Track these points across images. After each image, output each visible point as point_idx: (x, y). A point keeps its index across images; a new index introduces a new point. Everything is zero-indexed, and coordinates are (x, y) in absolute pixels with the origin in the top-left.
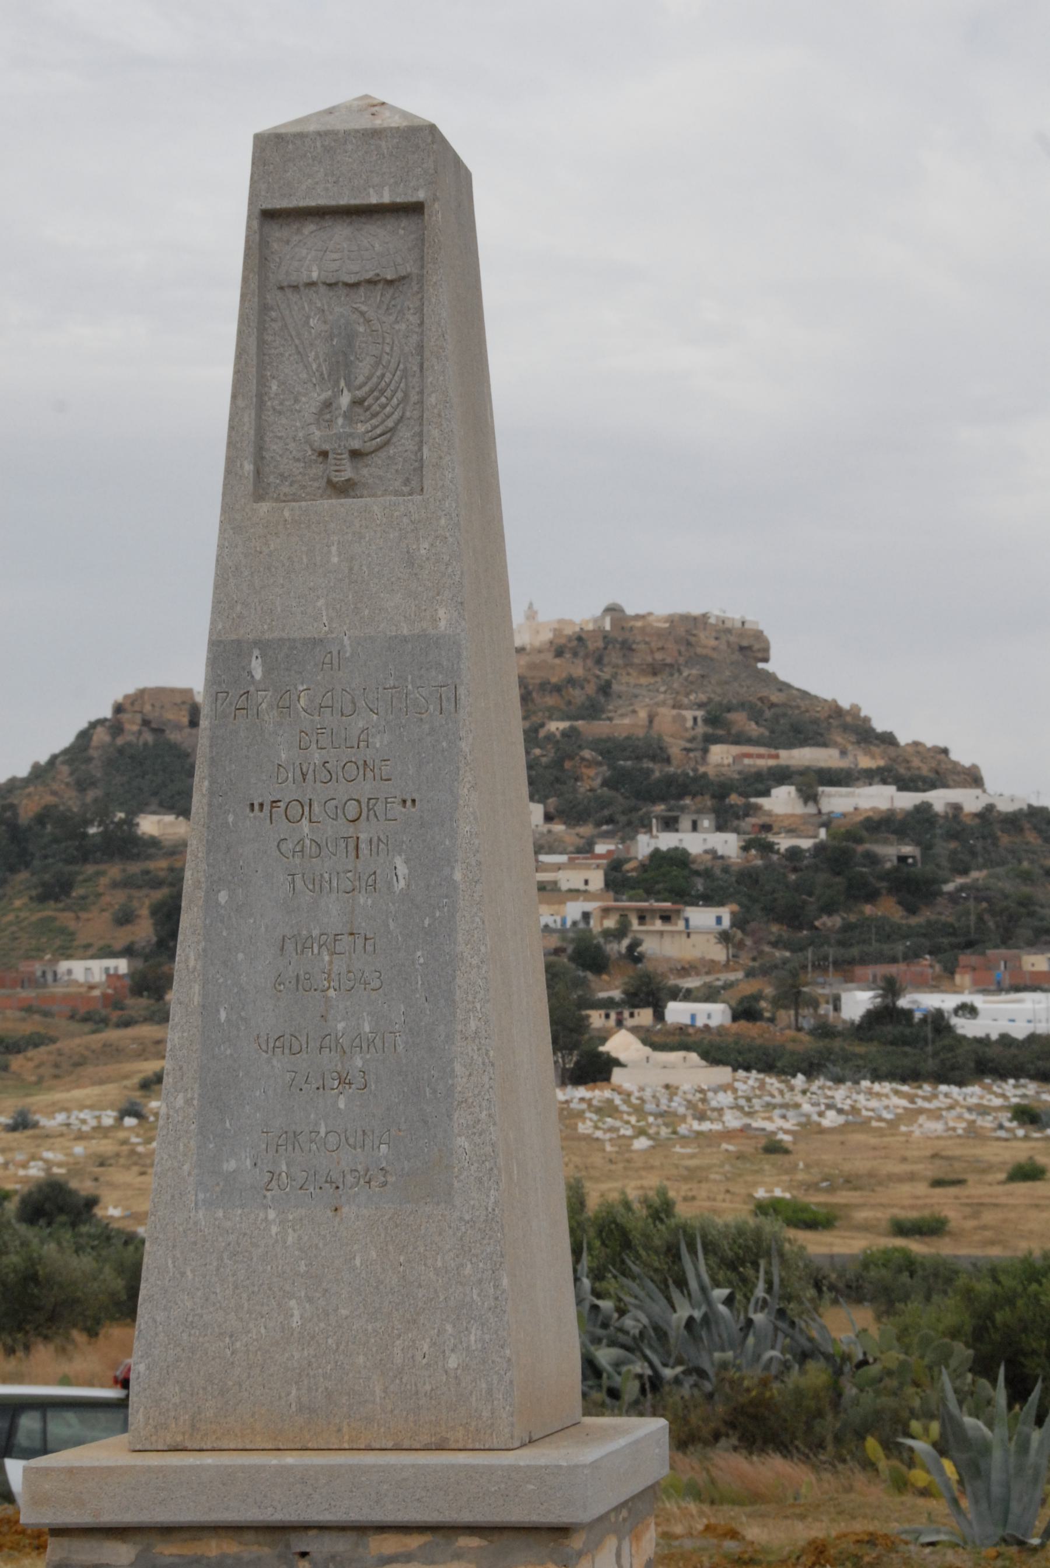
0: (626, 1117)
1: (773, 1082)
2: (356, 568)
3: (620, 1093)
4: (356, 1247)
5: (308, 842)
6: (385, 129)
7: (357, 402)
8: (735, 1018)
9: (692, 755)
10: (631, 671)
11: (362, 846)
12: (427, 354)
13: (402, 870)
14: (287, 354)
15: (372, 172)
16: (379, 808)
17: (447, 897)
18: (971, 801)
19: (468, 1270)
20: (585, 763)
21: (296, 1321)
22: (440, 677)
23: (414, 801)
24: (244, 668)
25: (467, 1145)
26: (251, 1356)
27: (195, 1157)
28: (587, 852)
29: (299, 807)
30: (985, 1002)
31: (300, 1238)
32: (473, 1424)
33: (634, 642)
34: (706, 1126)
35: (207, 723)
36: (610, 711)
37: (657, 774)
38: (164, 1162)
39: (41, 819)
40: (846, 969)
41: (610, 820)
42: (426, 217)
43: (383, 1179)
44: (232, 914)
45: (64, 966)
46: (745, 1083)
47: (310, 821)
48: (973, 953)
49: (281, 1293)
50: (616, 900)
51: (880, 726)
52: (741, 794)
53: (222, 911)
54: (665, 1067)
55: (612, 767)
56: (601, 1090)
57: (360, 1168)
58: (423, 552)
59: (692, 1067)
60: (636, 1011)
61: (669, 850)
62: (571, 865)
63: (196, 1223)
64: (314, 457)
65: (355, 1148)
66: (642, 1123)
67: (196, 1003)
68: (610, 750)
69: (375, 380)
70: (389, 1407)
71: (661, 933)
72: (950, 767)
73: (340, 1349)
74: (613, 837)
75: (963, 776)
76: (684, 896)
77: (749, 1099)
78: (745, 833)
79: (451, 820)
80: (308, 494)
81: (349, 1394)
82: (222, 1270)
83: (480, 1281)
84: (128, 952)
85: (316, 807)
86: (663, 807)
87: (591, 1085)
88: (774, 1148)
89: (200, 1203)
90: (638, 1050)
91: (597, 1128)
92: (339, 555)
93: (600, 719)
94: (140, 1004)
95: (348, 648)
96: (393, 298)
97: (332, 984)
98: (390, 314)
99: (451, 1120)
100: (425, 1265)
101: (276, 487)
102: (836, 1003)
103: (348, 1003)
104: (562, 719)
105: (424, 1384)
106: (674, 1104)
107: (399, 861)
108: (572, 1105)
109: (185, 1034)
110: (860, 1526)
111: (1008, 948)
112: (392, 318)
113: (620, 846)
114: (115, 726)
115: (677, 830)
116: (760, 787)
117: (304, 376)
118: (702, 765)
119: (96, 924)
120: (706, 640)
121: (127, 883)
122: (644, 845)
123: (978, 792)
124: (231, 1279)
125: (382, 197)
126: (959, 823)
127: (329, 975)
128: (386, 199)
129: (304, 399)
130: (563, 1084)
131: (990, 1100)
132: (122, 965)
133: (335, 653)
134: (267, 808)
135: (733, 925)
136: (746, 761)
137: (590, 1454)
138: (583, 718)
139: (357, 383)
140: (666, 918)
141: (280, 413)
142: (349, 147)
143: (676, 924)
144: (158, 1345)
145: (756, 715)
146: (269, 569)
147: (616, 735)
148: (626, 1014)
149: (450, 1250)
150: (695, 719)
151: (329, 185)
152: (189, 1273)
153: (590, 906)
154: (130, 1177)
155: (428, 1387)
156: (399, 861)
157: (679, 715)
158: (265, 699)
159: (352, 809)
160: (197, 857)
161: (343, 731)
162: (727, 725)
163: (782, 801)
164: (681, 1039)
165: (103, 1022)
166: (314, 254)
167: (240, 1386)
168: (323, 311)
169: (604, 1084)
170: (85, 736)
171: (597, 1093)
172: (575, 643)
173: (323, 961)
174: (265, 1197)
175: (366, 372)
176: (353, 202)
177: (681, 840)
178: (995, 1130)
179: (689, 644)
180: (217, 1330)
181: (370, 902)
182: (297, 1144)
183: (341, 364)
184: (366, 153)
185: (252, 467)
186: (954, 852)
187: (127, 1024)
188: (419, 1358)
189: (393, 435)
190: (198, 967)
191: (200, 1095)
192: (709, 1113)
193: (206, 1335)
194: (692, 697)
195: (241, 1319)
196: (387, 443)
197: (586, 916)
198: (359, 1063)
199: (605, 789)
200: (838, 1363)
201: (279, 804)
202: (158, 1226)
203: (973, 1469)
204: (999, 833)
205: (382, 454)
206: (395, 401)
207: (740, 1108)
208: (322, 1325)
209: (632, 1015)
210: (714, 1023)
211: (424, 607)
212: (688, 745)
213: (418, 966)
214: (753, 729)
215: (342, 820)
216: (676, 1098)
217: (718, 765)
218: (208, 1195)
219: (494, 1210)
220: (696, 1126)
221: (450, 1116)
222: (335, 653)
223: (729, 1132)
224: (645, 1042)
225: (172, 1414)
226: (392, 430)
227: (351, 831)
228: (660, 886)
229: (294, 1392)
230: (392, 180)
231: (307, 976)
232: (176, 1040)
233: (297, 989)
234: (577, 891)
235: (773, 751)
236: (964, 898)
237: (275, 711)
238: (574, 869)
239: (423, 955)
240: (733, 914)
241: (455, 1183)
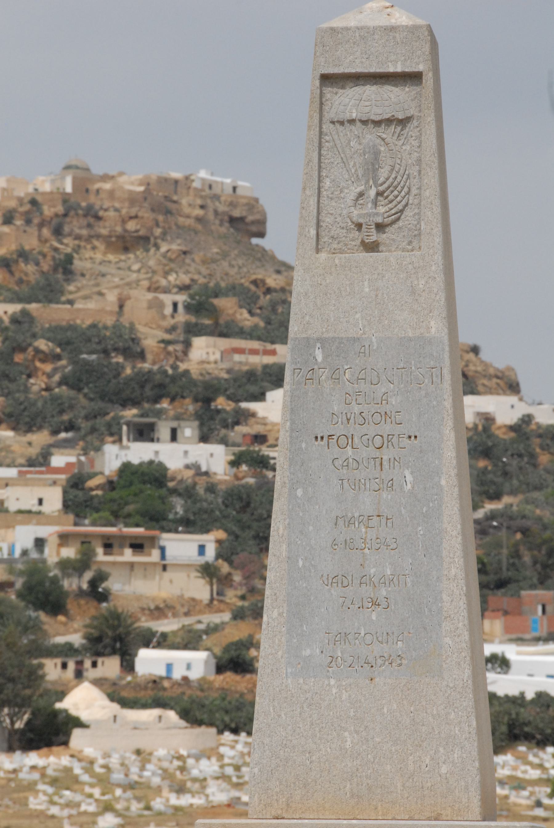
0: (87, 789)
2: (380, 295)
3: (80, 760)
4: (384, 702)
5: (351, 460)
6: (399, 27)
7: (379, 194)
8: (220, 669)
9: (171, 348)
10: (96, 243)
11: (385, 463)
12: (424, 166)
13: (409, 478)
14: (336, 163)
15: (390, 52)
16: (395, 440)
17: (436, 495)
19: (452, 716)
20: (41, 356)
21: (348, 744)
22: (432, 362)
23: (416, 437)
24: (310, 354)
25: (450, 642)
26: (322, 765)
27: (285, 647)
28: (41, 465)
29: (346, 439)
30: (519, 653)
31: (350, 696)
32: (457, 806)
33: (101, 208)
34: (185, 800)
35: (288, 387)
36: (71, 293)
37: (128, 371)
38: (266, 650)
41: (70, 427)
42: (424, 81)
43: (400, 662)
44: (305, 503)
46: (233, 747)
47: (352, 448)
48: (505, 595)
49: (339, 728)
50: (76, 524)
52: (229, 398)
53: (299, 501)
54: (135, 728)
55: (74, 362)
56: (58, 756)
57: (385, 655)
58: (421, 286)
59: (168, 728)
60: (100, 660)
61: (141, 464)
62: (22, 480)
64: (353, 227)
65: (382, 644)
66: (106, 797)
67: (284, 556)
68: (69, 339)
69: (391, 180)
70: (406, 795)
71: (132, 566)
72: (479, 369)
73: (376, 762)
74: (73, 447)
75: (495, 380)
76: (158, 519)
77: (237, 768)
78: (234, 445)
80: (349, 249)
81: (381, 787)
82: (303, 714)
83: (460, 722)
85: (356, 440)
86: (135, 411)
87: (45, 750)
89: (289, 675)
90: (104, 708)
91: (52, 803)
92: (369, 287)
93: (58, 302)
95: (375, 344)
96: (402, 130)
97: (367, 546)
98: (400, 140)
99: (440, 627)
100: (426, 712)
101: (329, 245)
103: (377, 557)
104: (11, 301)
105: (427, 782)
106: (146, 774)
107: (407, 473)
108: (21, 775)
109: (278, 574)
111: (548, 588)
112: (401, 142)
113: (83, 458)
115: (152, 440)
116: (253, 389)
117: (346, 176)
118: (182, 361)
123: (513, 399)
124: (308, 719)
125: (396, 68)
126: (489, 437)
127: (365, 540)
128: (399, 69)
129: (346, 191)
130: (11, 749)
131: (525, 772)
133: (367, 346)
134: (325, 439)
135: (219, 556)
136: (237, 357)
138: (38, 301)
139: (380, 182)
140: (138, 546)
141: (332, 199)
142: (376, 37)
143: (150, 555)
144: (265, 757)
145: (248, 300)
146: (326, 294)
147: (78, 322)
148: (88, 663)
149: (441, 704)
150: (175, 305)
151: (364, 60)
152: (283, 716)
153: (44, 531)
155: (429, 784)
156: (407, 473)
157: (156, 298)
158: (324, 374)
159: (378, 441)
160: (283, 468)
161: (372, 393)
162: (214, 312)
164: (154, 694)
166: (350, 101)
167: (316, 782)
168: (359, 137)
169: (61, 749)
171: (52, 759)
172: (27, 207)
173: (361, 532)
174: (328, 671)
175: (386, 175)
176: (378, 70)
177: (157, 453)
178: (531, 808)
179: (168, 212)
180: (301, 749)
181: (389, 497)
182: (347, 641)
183: (372, 167)
184: (387, 41)
186: (484, 471)
188: (423, 767)
189: (402, 214)
190: (285, 535)
191: (287, 611)
192: (189, 784)
193: (294, 752)
194: (172, 278)
195: (315, 743)
196: (398, 219)
197: (40, 543)
198: (384, 593)
199: (64, 388)
201: (333, 437)
202: (264, 688)
204: (538, 450)
205: (396, 226)
206: (403, 194)
208: (364, 747)
209: (94, 665)
210: (195, 674)
211: (422, 320)
212: (167, 337)
213: (419, 536)
214: (244, 318)
215: (371, 448)
216: (149, 766)
217: (203, 362)
218: (294, 670)
219: (467, 681)
220: (174, 800)
221: (440, 625)
222: (367, 346)
223: (213, 807)
224: (112, 697)
225: (275, 798)
226: (402, 211)
227: (377, 454)
228: (130, 508)
229: (348, 785)
230: (403, 58)
231: (352, 541)
232: (272, 577)
233: (346, 548)
234: (29, 512)
235: (269, 347)
236: (495, 527)
237: (330, 381)
238: (26, 485)
239: (422, 529)
240: (219, 542)
241: (444, 665)
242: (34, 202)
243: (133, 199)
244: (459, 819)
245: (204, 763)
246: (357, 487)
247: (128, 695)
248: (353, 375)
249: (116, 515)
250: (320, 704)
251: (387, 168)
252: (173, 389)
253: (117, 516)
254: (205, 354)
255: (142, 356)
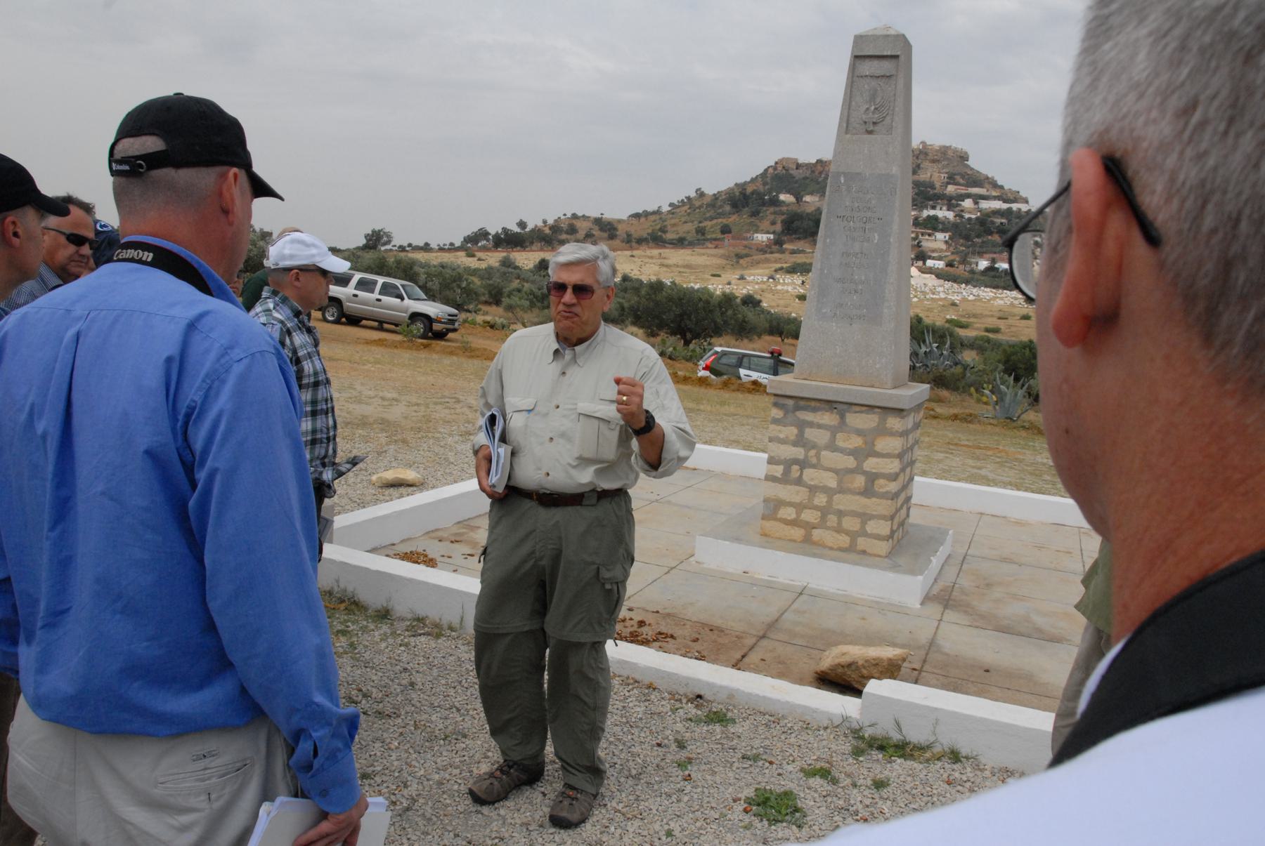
1: (955, 285)
18: (1024, 208)
39: (753, 193)
40: (981, 254)
51: (1000, 183)
76: (935, 229)
84: (774, 233)
88: (954, 304)
94: (775, 248)
102: (977, 264)
110: (967, 411)
114: (775, 168)
119: (765, 224)
120: (950, 153)
121: (775, 213)
132: (772, 236)
137: (911, 392)
145: (963, 177)
154: (770, 296)
158: (844, 188)
163: (968, 203)
165: (765, 252)
166: (868, 68)
170: (766, 170)
183: (873, 97)
187: (772, 253)
200: (965, 367)
203: (1001, 400)
214: (961, 181)
247: (923, 270)
253: (925, 228)
254: (951, 189)
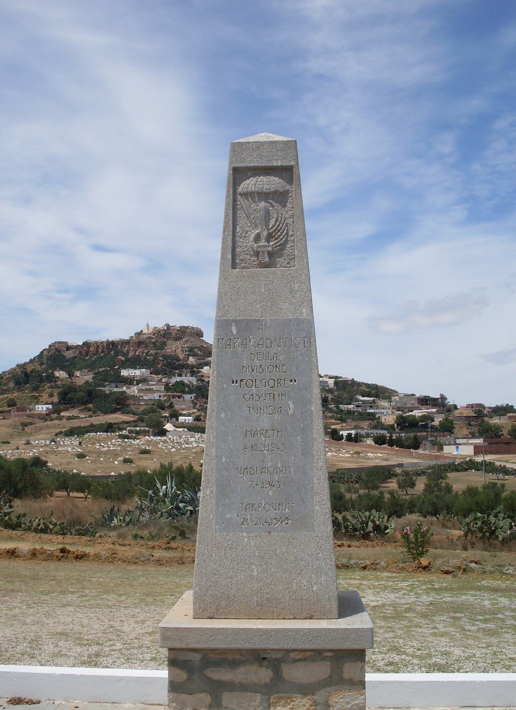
11: (276, 397)
13: (292, 406)
21: (255, 574)
23: (295, 381)
32: (323, 610)
45: (37, 406)
63: (216, 537)
68: (165, 357)
69: (276, 226)
79: (310, 387)
83: (325, 558)
84: (52, 403)
85: (258, 382)
107: (290, 403)
114: (49, 350)
121: (52, 387)
122: (175, 379)
132: (50, 406)
140: (179, 397)
141: (241, 238)
142: (265, 147)
156: (290, 403)
164: (182, 425)
165: (46, 420)
166: (250, 184)
170: (42, 353)
173: (262, 439)
181: (279, 418)
185: (231, 256)
198: (277, 478)
207: (196, 441)
208: (265, 575)
210: (190, 422)
221: (312, 498)
224: (174, 426)
225: (209, 606)
242: (159, 331)
243: (178, 330)
244: (325, 618)
245: (192, 439)
246: (259, 412)
248: (255, 343)
249: (175, 391)
250: (237, 548)
251: (274, 219)
252: (186, 367)
253: (175, 391)
254: (192, 360)
255: (180, 360)
